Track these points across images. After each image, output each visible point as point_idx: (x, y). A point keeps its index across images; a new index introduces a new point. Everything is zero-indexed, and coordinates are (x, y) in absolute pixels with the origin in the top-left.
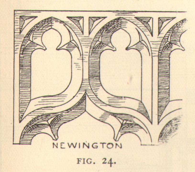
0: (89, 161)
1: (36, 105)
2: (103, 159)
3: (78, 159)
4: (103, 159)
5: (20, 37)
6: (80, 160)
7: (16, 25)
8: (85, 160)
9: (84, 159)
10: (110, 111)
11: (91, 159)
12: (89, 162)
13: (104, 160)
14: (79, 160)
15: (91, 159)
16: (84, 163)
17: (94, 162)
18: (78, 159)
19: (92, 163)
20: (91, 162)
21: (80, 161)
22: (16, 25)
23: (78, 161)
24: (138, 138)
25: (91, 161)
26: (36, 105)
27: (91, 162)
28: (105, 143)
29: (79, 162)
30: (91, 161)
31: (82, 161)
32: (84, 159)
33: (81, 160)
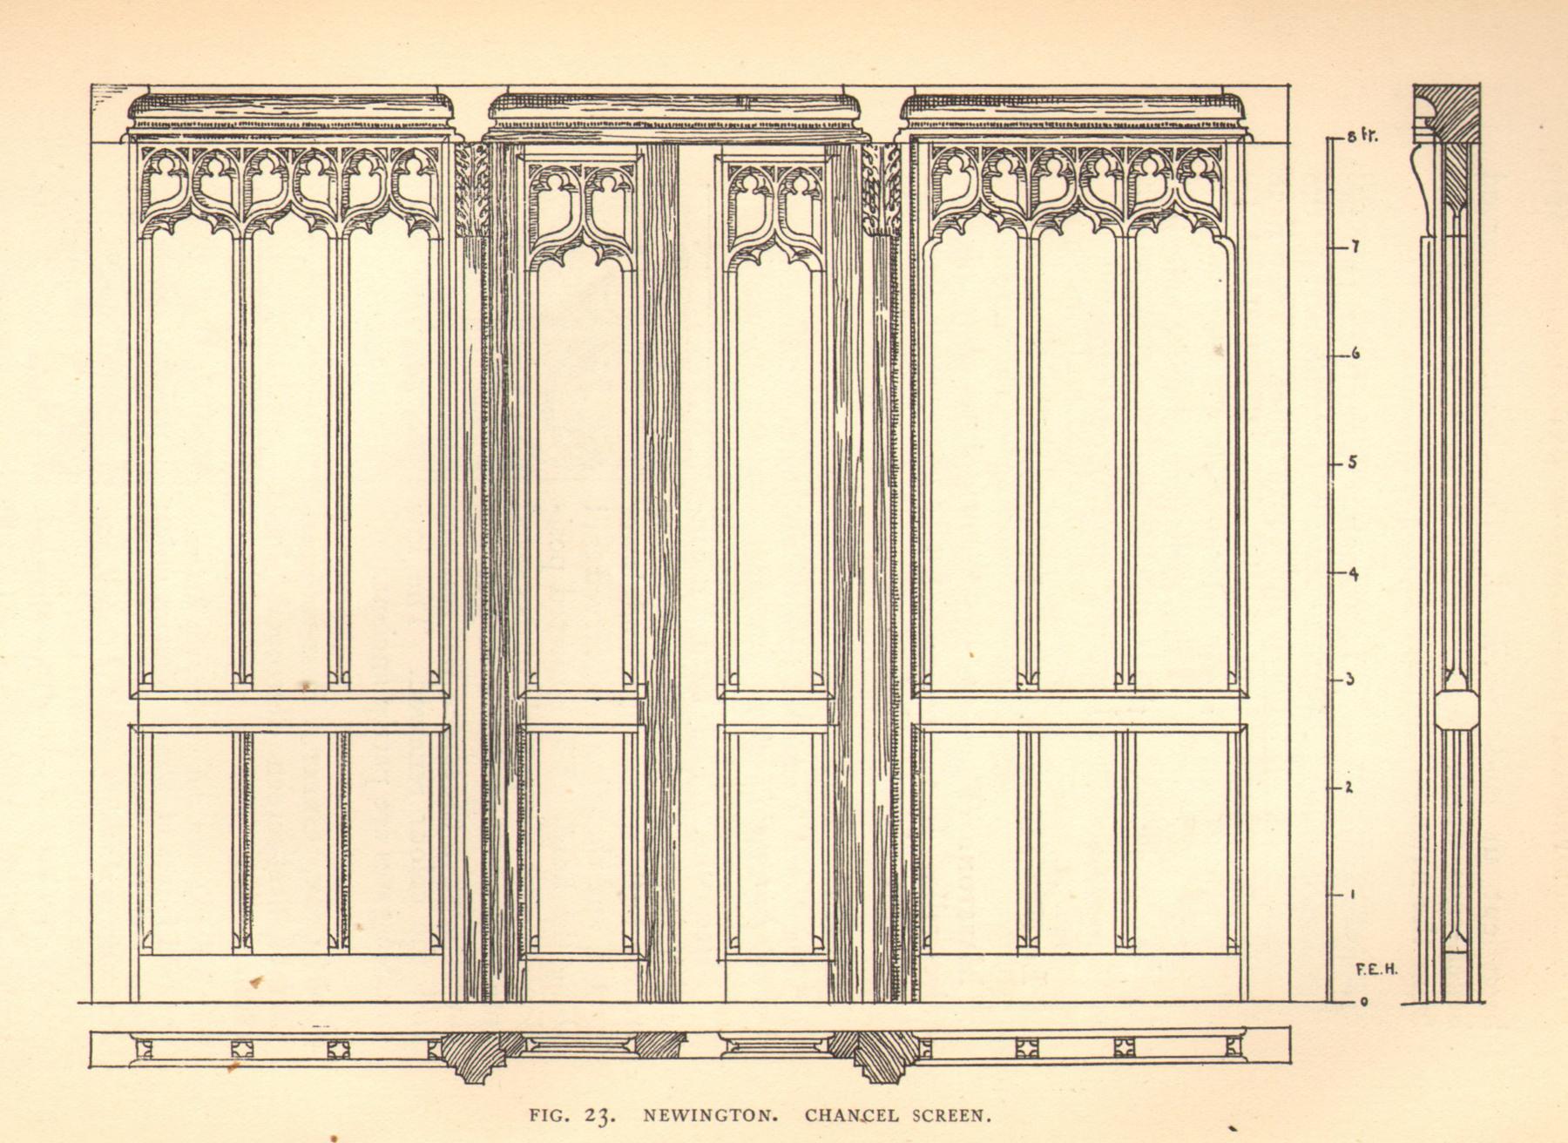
0: (556, 1115)
1: (749, 1115)
2: (587, 1111)
3: (532, 1110)
4: (587, 1111)
5: (662, 345)
6: (665, 1112)
7: (738, 737)
8: (548, 1114)
9: (545, 1111)
10: (709, 216)
11: (561, 1112)
12: (721, 1117)
13: (589, 1112)
14: (533, 1113)
15: (561, 1112)
16: (545, 1120)
17: (567, 1117)
18: (532, 1110)
19: (563, 1119)
20: (560, 1118)
21: (536, 1115)
22: (738, 737)
23: (532, 1115)
24: (597, 224)
25: (559, 1115)
26: (749, 1115)
27: (560, 1118)
28: (740, 1111)
29: (535, 1117)
30: (559, 1115)
31: (541, 1114)
32: (545, 1111)
33: (539, 1113)
